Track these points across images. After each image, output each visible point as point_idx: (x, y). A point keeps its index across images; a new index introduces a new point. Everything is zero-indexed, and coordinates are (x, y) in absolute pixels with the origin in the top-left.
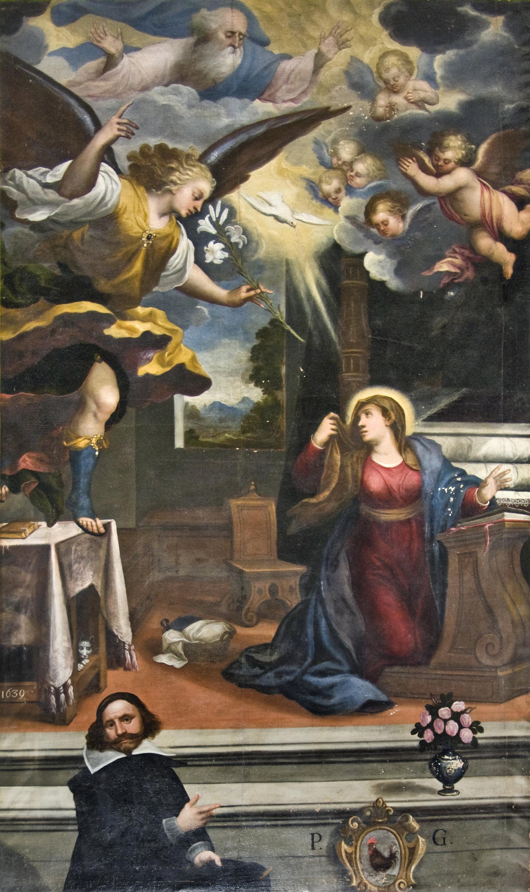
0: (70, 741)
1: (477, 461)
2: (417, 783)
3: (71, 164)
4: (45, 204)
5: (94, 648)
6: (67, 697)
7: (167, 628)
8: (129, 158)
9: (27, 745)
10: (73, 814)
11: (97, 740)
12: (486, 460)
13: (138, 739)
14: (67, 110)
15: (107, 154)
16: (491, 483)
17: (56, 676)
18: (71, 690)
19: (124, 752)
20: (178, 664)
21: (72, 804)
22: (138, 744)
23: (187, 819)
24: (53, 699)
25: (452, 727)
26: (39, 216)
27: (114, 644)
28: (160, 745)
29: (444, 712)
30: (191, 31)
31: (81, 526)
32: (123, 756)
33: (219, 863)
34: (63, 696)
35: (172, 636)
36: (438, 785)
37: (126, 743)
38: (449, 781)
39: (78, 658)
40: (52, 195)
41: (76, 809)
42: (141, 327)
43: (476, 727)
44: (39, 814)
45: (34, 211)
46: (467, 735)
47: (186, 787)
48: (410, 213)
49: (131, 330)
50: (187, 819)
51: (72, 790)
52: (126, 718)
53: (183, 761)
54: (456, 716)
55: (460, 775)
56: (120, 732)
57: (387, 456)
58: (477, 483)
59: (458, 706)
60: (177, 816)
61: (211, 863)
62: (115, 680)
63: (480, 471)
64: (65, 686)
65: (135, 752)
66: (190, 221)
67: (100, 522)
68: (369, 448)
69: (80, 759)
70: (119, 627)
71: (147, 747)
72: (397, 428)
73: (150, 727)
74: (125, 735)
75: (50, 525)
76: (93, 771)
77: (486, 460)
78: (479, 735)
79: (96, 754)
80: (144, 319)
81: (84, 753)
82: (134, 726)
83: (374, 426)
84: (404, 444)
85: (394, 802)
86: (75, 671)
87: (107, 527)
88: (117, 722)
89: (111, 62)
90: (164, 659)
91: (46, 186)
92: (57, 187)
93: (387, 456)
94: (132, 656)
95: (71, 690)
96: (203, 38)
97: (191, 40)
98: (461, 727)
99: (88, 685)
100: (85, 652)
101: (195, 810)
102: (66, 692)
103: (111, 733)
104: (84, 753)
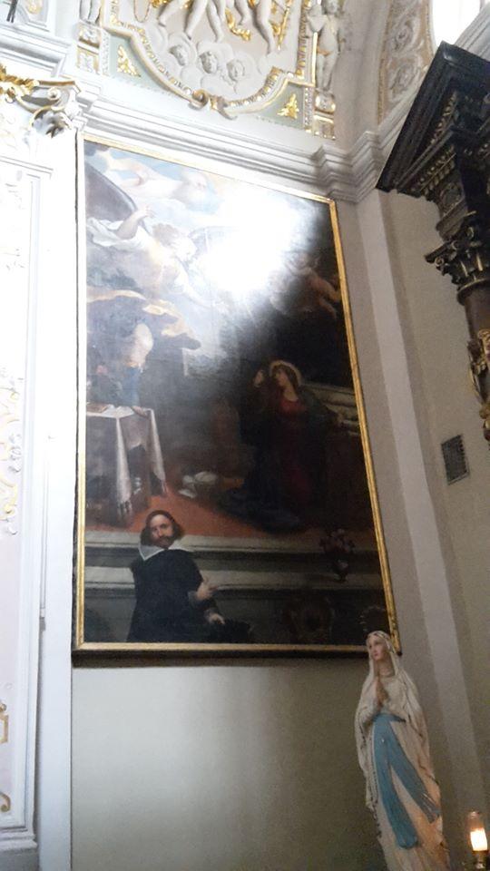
0: (130, 538)
1: (332, 404)
2: (196, 537)
3: (122, 225)
4: (109, 238)
5: (143, 481)
6: (128, 511)
7: (185, 474)
8: (154, 227)
9: (103, 540)
10: (133, 586)
11: (147, 539)
12: (337, 404)
13: (171, 540)
14: (119, 197)
15: (141, 222)
16: (341, 416)
17: (120, 498)
18: (130, 506)
19: (163, 547)
20: (191, 496)
21: (132, 580)
22: (171, 543)
23: (203, 591)
24: (119, 511)
25: (339, 544)
26: (107, 244)
27: (155, 482)
28: (26, 145)
29: (333, 534)
30: (182, 178)
31: (134, 410)
32: (162, 550)
33: (223, 622)
34: (125, 510)
35: (188, 479)
36: (336, 576)
37: (164, 542)
38: (343, 574)
39: (134, 487)
40: (113, 235)
41: (135, 584)
42: (163, 311)
43: (351, 543)
44: (111, 586)
45: (104, 241)
46: (347, 548)
47: (201, 572)
48: (391, 61)
49: (159, 311)
50: (203, 591)
51: (133, 570)
52: (163, 526)
53: (199, 555)
54: (341, 537)
55: (346, 572)
56: (160, 535)
57: (291, 396)
58: (335, 415)
59: (341, 531)
60: (197, 590)
61: (217, 622)
62: (155, 502)
63: (335, 409)
64: (127, 503)
65: (170, 548)
66: (186, 264)
67: (145, 410)
68: (282, 389)
69: (135, 551)
70: (157, 471)
71: (176, 546)
72: (293, 381)
73: (178, 533)
74: (162, 537)
75: (116, 406)
76: (145, 558)
77: (337, 404)
78: (354, 549)
79: (147, 548)
80: (164, 306)
81: (139, 547)
82: (168, 532)
83: (282, 378)
84: (298, 390)
85: (317, 586)
86: (132, 494)
87: (149, 412)
88: (159, 529)
89: (141, 182)
90: (184, 492)
91: (109, 230)
92: (116, 232)
93: (291, 396)
94: (165, 489)
95: (130, 506)
96: (187, 183)
97: (181, 183)
98: (344, 543)
99: (140, 503)
100: (138, 484)
101: (207, 587)
102: (127, 506)
103: (155, 535)
104: (139, 547)
